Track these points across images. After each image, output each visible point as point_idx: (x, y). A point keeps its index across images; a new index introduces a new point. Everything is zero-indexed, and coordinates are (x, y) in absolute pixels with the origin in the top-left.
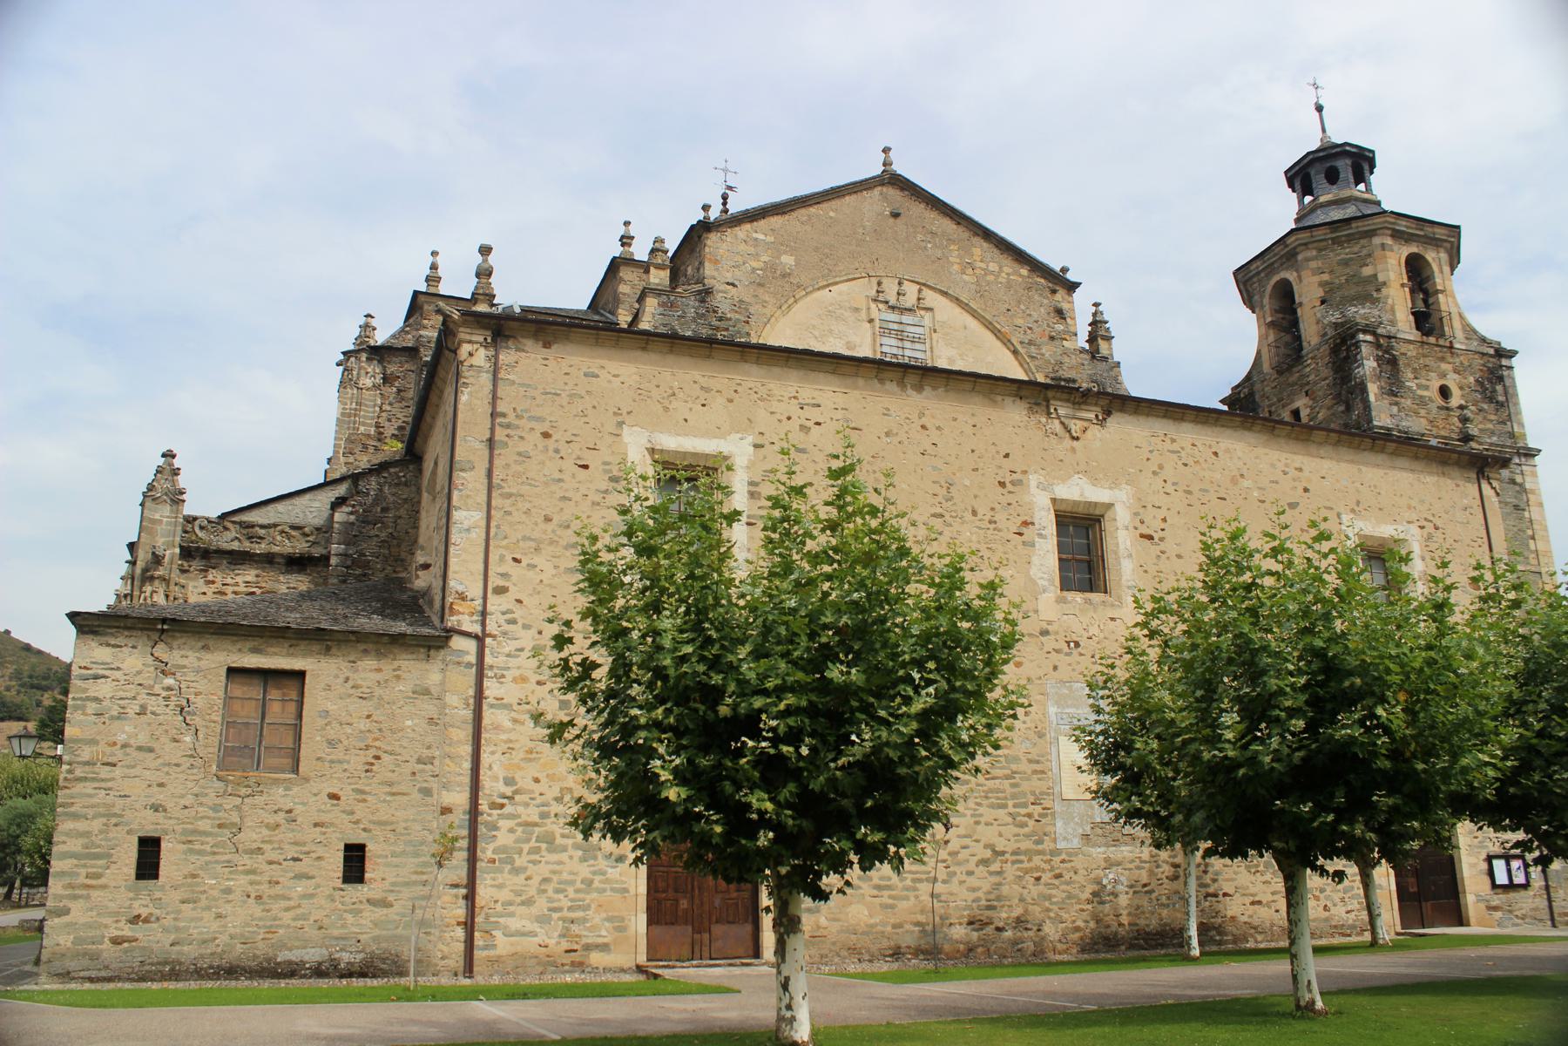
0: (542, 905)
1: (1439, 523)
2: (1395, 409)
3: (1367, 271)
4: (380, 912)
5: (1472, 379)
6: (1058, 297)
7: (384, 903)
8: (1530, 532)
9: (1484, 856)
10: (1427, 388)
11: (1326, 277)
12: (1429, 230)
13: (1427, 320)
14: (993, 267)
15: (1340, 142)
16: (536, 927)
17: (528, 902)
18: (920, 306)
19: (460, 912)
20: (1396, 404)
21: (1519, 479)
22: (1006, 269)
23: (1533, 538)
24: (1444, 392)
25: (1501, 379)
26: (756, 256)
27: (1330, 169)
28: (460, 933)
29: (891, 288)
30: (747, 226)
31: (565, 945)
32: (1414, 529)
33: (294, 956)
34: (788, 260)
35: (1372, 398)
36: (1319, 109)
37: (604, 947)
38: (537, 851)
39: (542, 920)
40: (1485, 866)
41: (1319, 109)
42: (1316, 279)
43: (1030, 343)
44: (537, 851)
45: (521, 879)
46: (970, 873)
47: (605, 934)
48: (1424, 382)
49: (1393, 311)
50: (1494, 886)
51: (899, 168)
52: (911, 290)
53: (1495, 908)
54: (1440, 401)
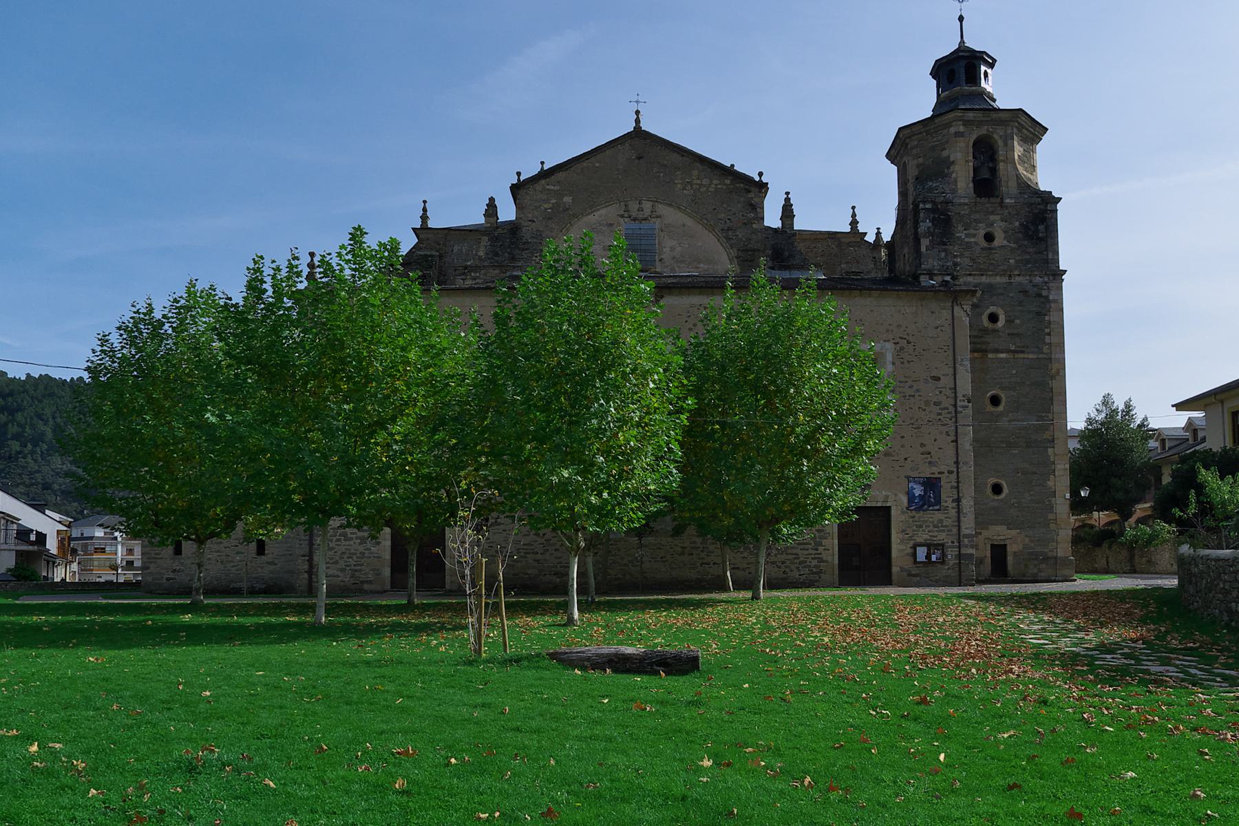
0: (342, 564)
1: (911, 339)
2: (943, 254)
3: (945, 154)
4: (272, 567)
5: (1017, 224)
6: (751, 195)
7: (273, 563)
8: (1047, 330)
9: (912, 543)
10: (974, 236)
11: (921, 160)
12: (994, 115)
13: (986, 185)
14: (706, 181)
15: (977, 47)
16: (339, 573)
17: (336, 563)
18: (654, 215)
19: (306, 567)
20: (945, 250)
21: (1044, 293)
22: (715, 182)
23: (1049, 334)
24: (989, 237)
25: (1043, 220)
26: (547, 201)
27: (960, 71)
28: (306, 575)
29: (634, 206)
30: (543, 182)
31: (352, 581)
32: (889, 345)
33: (237, 585)
34: (567, 199)
35: (923, 249)
36: (961, 19)
37: (370, 582)
38: (339, 540)
39: (342, 570)
40: (910, 551)
41: (961, 19)
42: (915, 162)
43: (729, 229)
44: (339, 540)
45: (331, 553)
46: (557, 550)
47: (371, 577)
48: (972, 231)
49: (956, 181)
50: (915, 562)
51: (645, 126)
52: (647, 206)
53: (915, 575)
54: (984, 244)
